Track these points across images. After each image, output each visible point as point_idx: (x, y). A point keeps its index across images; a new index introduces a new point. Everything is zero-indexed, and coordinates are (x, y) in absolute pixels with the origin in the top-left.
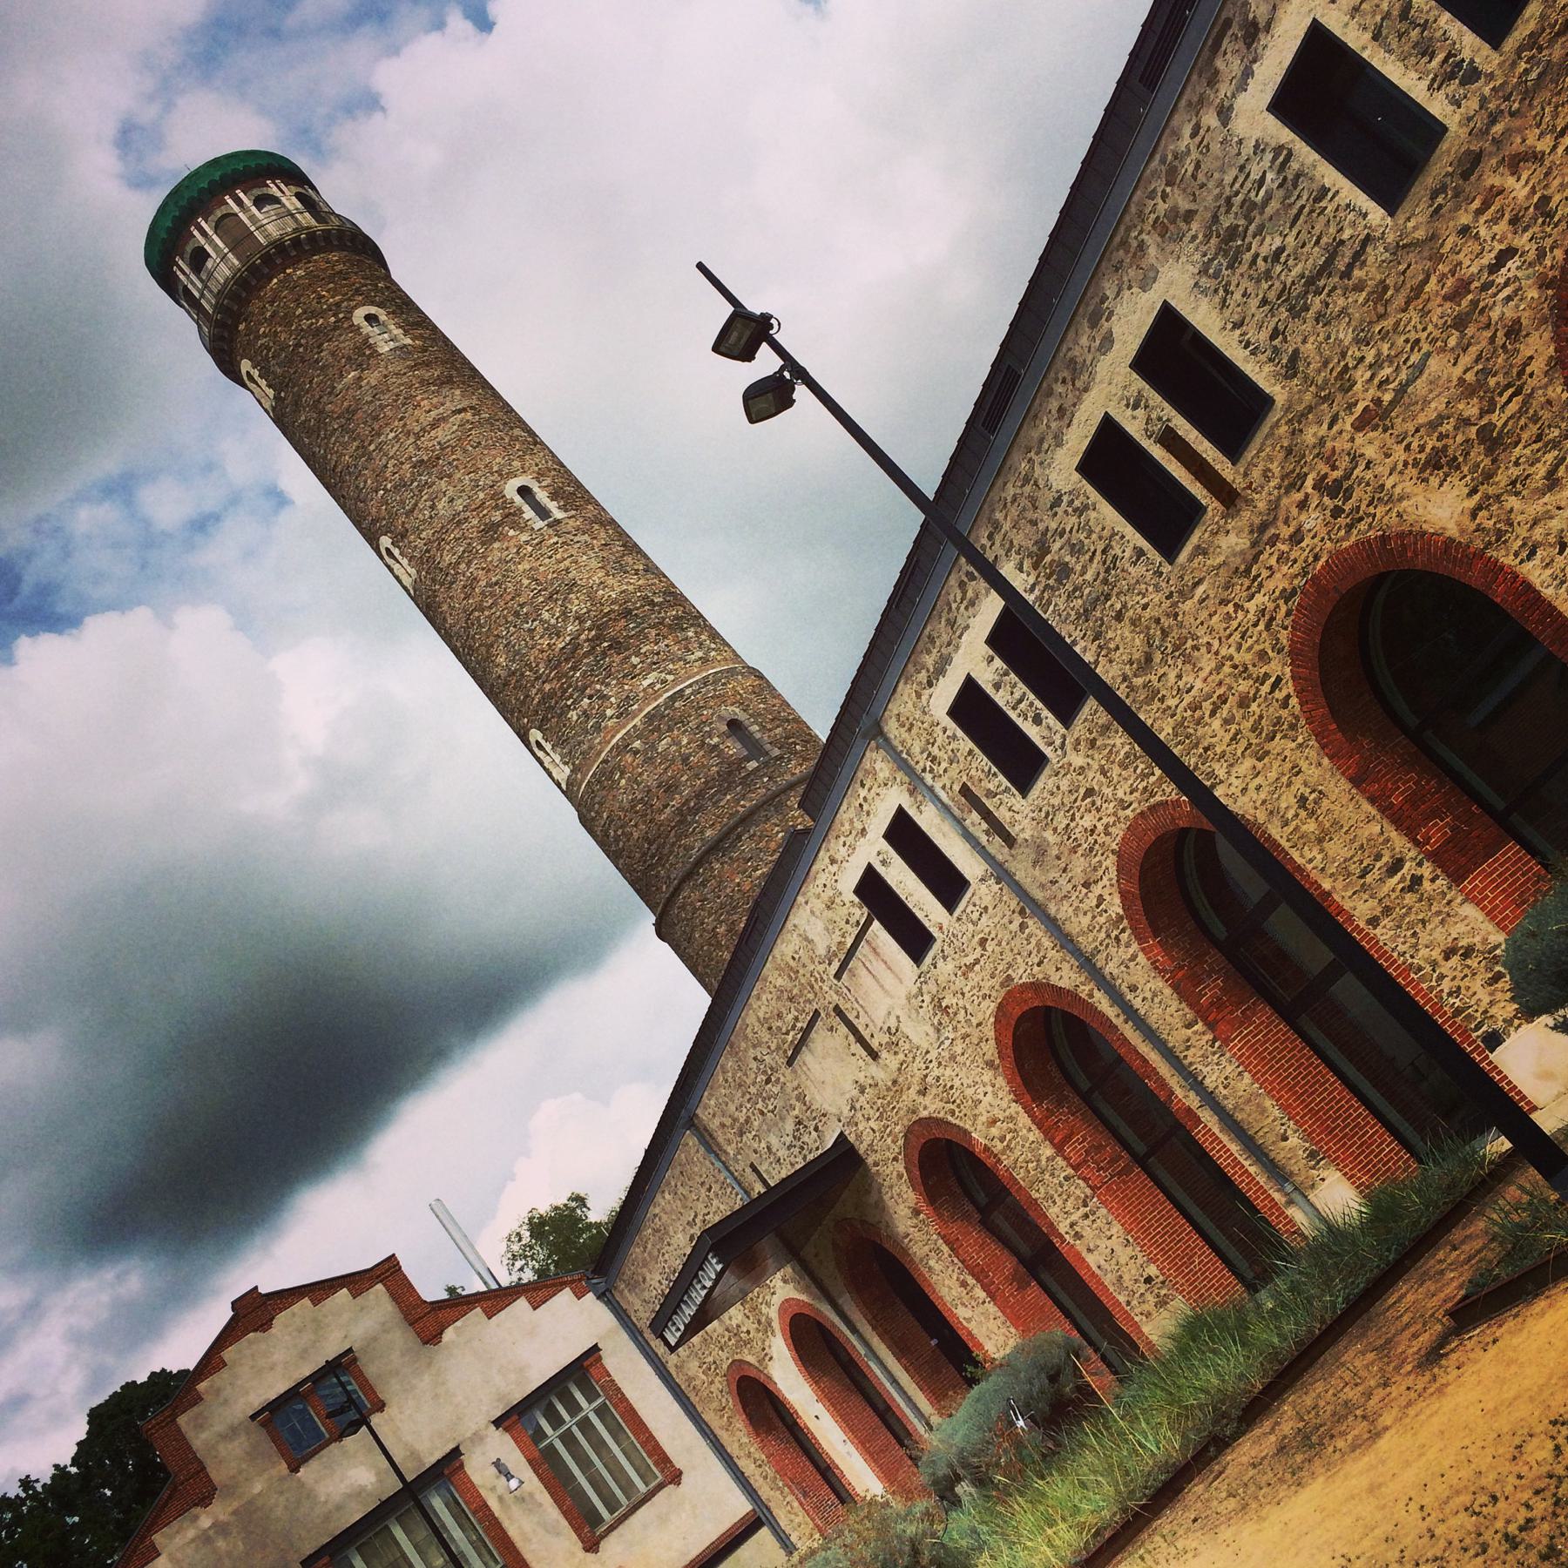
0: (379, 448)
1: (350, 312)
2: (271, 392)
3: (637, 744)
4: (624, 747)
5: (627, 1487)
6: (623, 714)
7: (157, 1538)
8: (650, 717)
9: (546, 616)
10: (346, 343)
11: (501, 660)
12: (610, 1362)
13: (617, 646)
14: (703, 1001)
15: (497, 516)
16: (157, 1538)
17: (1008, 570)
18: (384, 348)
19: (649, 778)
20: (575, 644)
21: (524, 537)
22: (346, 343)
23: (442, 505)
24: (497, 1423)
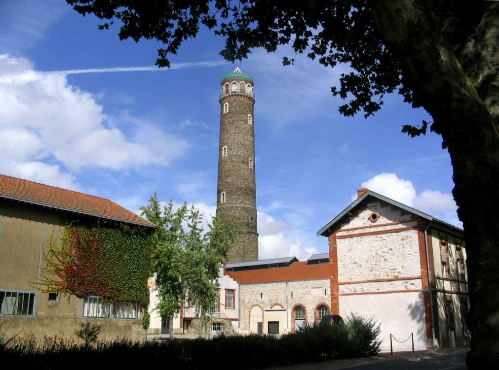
0: (238, 136)
1: (248, 114)
2: (228, 111)
3: (240, 209)
4: (237, 207)
5: (299, 317)
6: (241, 203)
7: (258, 25)
8: (244, 207)
9: (241, 180)
10: (245, 117)
11: (230, 180)
12: (236, 292)
13: (247, 193)
14: (357, 198)
15: (246, 161)
16: (258, 25)
17: (67, 314)
18: (249, 123)
19: (237, 215)
20: (242, 188)
21: (247, 167)
22: (245, 117)
23: (240, 152)
24: (225, 289)
